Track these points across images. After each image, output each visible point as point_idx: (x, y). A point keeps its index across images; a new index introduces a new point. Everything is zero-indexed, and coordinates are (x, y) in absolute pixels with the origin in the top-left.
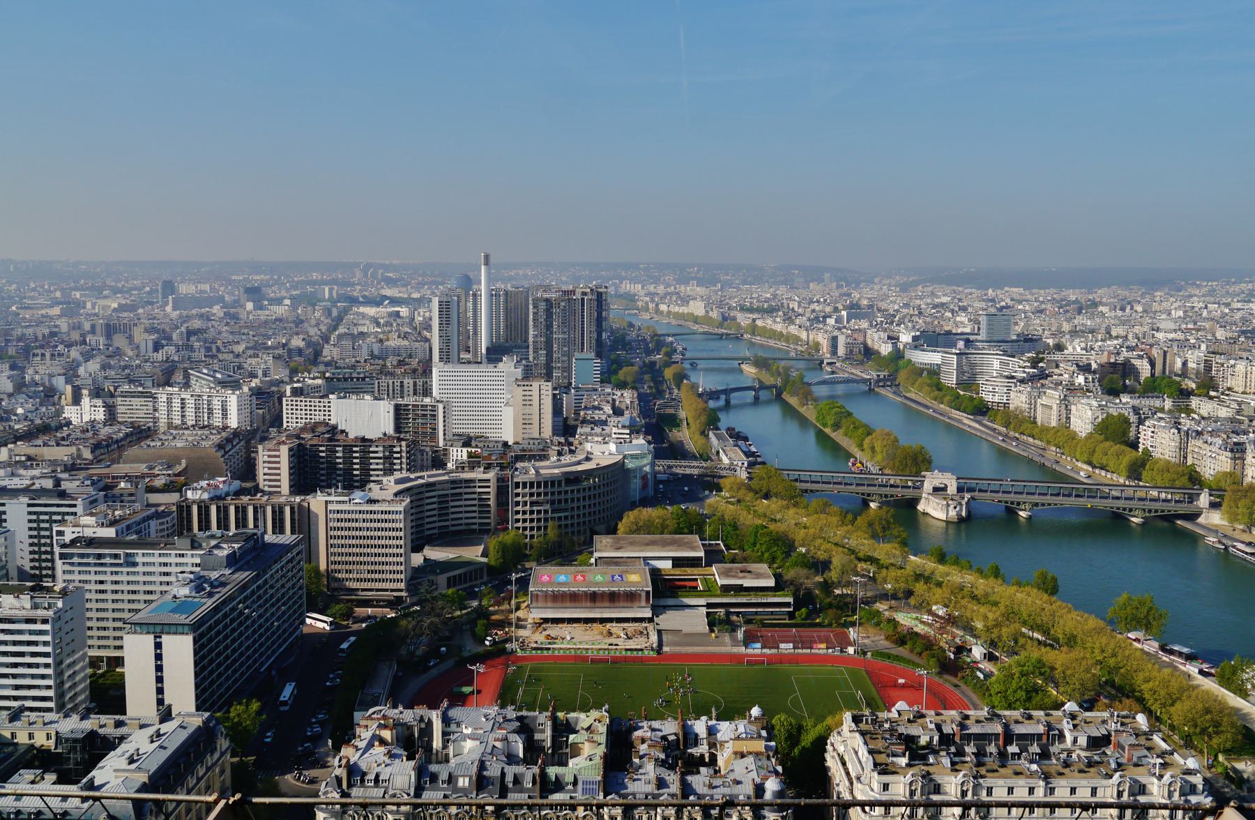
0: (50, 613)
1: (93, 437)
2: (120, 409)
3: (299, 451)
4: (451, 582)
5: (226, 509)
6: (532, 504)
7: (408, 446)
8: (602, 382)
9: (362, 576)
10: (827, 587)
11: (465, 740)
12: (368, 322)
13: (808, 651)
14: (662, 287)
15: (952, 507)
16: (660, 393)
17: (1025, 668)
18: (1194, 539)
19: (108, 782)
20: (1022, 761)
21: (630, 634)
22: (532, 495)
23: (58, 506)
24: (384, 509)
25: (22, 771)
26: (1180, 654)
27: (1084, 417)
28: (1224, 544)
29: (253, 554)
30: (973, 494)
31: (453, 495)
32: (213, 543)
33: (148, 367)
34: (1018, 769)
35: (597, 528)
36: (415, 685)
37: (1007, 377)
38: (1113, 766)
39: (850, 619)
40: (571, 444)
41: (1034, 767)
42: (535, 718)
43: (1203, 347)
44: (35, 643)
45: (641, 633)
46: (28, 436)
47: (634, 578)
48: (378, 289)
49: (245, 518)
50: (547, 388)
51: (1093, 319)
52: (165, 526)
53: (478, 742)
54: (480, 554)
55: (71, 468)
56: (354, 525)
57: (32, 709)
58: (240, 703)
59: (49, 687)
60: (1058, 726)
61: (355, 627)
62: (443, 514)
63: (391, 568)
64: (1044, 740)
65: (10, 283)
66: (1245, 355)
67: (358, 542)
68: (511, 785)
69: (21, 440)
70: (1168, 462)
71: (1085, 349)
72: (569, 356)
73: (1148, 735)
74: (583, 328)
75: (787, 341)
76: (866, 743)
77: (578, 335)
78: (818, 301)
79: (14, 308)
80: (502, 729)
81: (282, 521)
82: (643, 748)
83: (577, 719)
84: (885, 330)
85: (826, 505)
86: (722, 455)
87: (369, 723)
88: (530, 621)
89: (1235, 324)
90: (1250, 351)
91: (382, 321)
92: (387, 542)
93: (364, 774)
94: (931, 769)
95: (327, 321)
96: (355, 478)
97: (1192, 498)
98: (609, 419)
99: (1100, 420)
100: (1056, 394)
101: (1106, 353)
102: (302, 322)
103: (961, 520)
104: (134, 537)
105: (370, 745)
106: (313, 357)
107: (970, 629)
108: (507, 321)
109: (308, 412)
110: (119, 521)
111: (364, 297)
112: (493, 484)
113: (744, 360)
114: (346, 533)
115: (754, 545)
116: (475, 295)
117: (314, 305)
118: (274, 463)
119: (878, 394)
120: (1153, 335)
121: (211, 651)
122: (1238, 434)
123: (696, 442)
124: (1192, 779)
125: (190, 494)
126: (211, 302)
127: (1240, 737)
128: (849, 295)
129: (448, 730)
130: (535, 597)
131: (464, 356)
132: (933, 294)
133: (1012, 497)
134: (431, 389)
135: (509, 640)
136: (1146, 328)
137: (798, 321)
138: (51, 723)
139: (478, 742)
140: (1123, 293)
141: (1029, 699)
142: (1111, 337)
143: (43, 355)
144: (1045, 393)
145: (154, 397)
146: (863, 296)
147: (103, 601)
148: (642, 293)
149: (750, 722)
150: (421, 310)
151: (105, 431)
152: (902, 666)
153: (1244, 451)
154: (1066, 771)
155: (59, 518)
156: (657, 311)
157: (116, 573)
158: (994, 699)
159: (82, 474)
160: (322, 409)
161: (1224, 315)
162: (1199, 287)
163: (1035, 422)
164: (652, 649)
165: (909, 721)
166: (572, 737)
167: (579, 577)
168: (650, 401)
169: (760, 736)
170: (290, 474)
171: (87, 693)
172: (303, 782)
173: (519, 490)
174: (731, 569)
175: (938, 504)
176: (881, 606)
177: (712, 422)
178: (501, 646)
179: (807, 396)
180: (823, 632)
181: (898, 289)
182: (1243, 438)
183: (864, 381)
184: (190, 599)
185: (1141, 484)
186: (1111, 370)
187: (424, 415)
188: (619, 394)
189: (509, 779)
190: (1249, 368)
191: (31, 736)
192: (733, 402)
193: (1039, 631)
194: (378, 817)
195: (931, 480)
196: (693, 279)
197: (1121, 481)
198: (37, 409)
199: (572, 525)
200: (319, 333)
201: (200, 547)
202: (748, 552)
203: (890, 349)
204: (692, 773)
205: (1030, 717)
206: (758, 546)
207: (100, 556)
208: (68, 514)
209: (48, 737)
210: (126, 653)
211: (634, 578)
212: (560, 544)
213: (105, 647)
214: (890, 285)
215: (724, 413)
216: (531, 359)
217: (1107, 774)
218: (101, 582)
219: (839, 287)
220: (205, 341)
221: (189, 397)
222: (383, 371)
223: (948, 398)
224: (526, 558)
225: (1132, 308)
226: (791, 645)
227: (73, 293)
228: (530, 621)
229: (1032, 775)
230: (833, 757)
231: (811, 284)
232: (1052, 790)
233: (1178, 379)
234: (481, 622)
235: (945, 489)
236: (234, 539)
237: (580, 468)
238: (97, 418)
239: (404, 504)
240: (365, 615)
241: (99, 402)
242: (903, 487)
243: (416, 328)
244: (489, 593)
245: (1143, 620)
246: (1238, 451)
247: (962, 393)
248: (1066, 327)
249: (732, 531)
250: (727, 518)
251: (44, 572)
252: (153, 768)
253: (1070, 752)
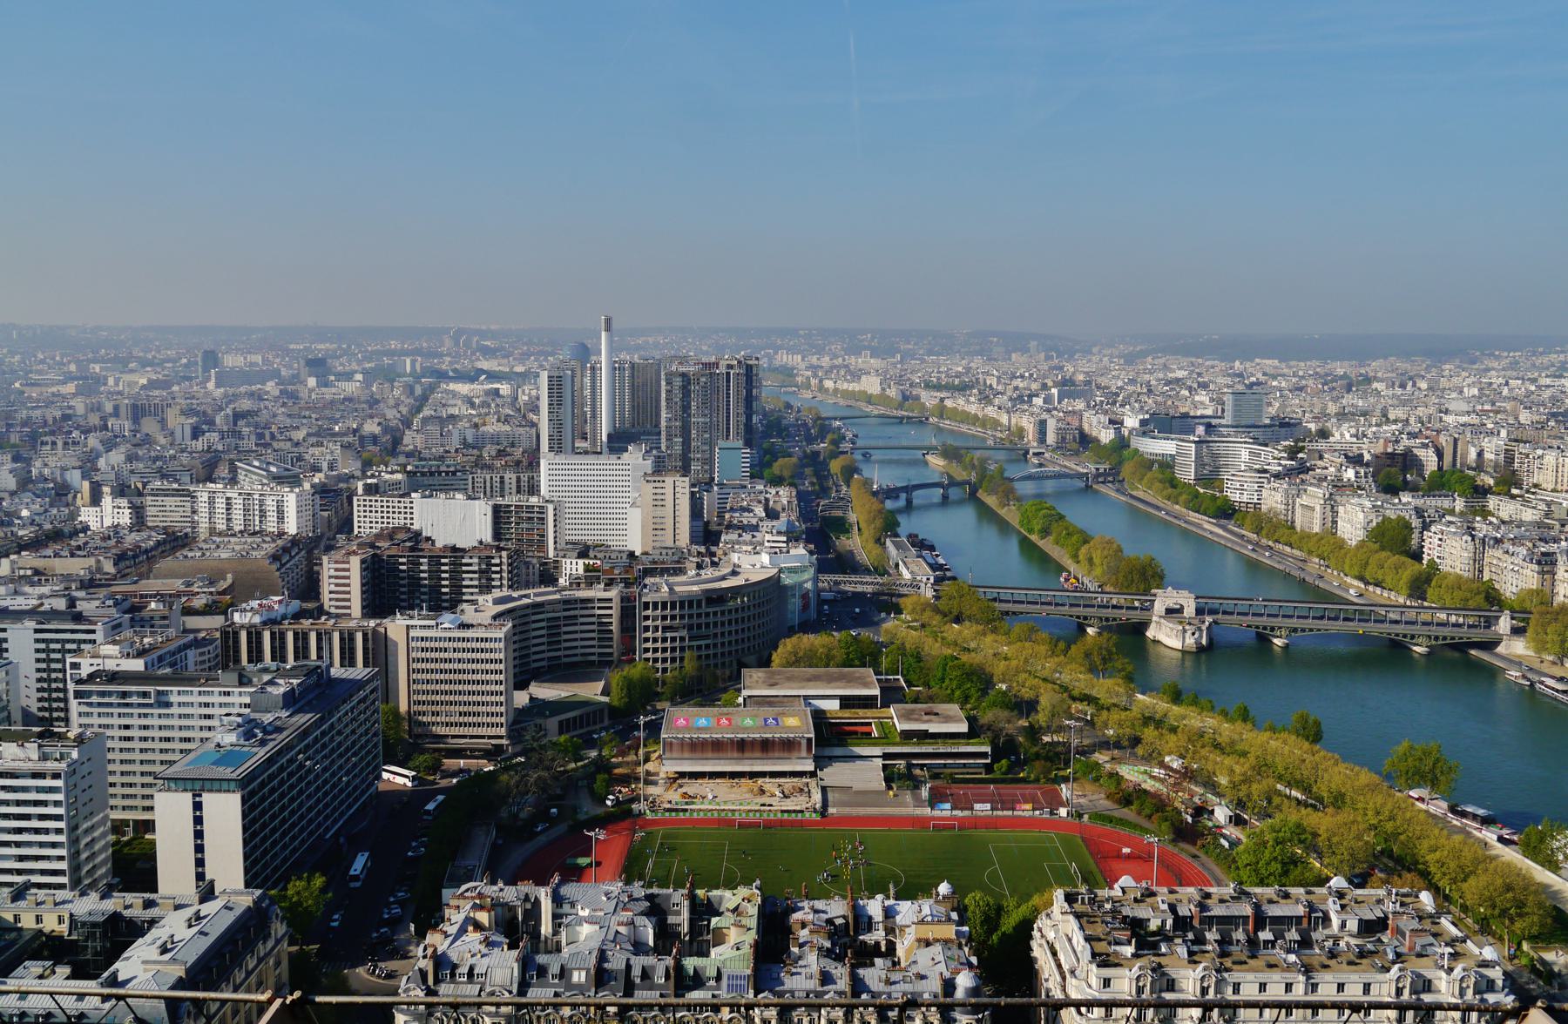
0: (63, 765)
1: (116, 546)
2: (151, 511)
3: (373, 563)
4: (564, 727)
5: (282, 636)
6: (665, 629)
7: (509, 557)
8: (752, 477)
9: (452, 719)
10: (1033, 732)
11: (581, 925)
12: (459, 402)
13: (1010, 813)
14: (827, 359)
15: (1189, 633)
16: (824, 491)
17: (1281, 835)
18: (1491, 673)
19: (135, 977)
20: (1277, 950)
21: (787, 792)
22: (664, 618)
23: (73, 631)
24: (480, 635)
25: (27, 963)
26: (1475, 817)
27: (1354, 521)
28: (1529, 680)
29: (317, 692)
30: (1215, 617)
31: (566, 618)
32: (266, 678)
33: (185, 458)
34: (1272, 960)
35: (746, 660)
36: (518, 855)
37: (1259, 471)
38: (1391, 956)
39: (1062, 773)
40: (713, 554)
41: (1292, 958)
42: (669, 897)
43: (1503, 433)
44: (44, 803)
45: (801, 790)
46: (35, 545)
47: (792, 722)
48: (472, 361)
49: (306, 647)
50: (684, 485)
51: (1365, 398)
52: (206, 657)
53: (597, 927)
54: (599, 692)
56: (442, 655)
57: (40, 886)
58: (300, 878)
59: (61, 858)
60: (1322, 907)
61: (444, 783)
62: (554, 642)
63: (489, 709)
64: (1305, 924)
65: (12, 353)
66: (1555, 443)
67: (447, 676)
68: (638, 981)
69: (26, 550)
70: (1459, 577)
71: (1356, 436)
72: (711, 444)
73: (1434, 918)
74: (728, 409)
75: (984, 426)
76: (1082, 928)
77: (722, 419)
78: (1022, 376)
79: (17, 385)
80: (627, 910)
81: (352, 650)
82: (804, 934)
83: (721, 898)
84: (1106, 412)
85: (1032, 630)
86: (902, 568)
87: (461, 902)
88: (662, 775)
89: (1543, 404)
90: (1562, 438)
91: (477, 401)
92: (484, 677)
93: (455, 967)
94: (1163, 960)
95: (408, 401)
96: (444, 597)
97: (1490, 622)
98: (761, 524)
99: (1374, 524)
100: (1319, 492)
101: (1382, 441)
102: (377, 402)
103: (1201, 649)
104: (168, 670)
105: (462, 931)
106: (392, 445)
107: (1212, 786)
108: (633, 401)
109: (385, 515)
110: (149, 650)
111: (455, 370)
112: (616, 604)
113: (930, 449)
114: (433, 666)
115: (943, 680)
116: (593, 369)
117: (392, 381)
118: (342, 578)
119: (1097, 492)
120: (1441, 418)
121: (263, 813)
122: (1547, 542)
123: (870, 552)
124: (1489, 973)
125: (237, 617)
126: (263, 377)
127: (1549, 921)
128: (1061, 368)
129: (560, 911)
130: (669, 746)
131: (580, 444)
132: (1165, 367)
133: (1264, 621)
134: (539, 486)
135: (636, 799)
136: (1432, 410)
137: (996, 401)
138: (64, 902)
139: (597, 927)
140: (1403, 366)
141: (1286, 873)
142: (1388, 421)
143: (54, 443)
144: (1305, 491)
145: (192, 496)
146: (1078, 370)
147: (128, 750)
148: (802, 366)
149: (937, 902)
150: (526, 388)
151: (131, 539)
152: (1126, 831)
153: (1554, 563)
154: (1332, 963)
155: (74, 646)
156: (821, 388)
157: (146, 716)
158: (1241, 872)
159: (103, 592)
160: (403, 510)
161: (1529, 394)
162: (1498, 358)
163: (1293, 527)
164: (815, 811)
165: (1136, 900)
166: (714, 921)
167: (724, 721)
168: (812, 501)
169: (949, 920)
170: (363, 592)
171: (109, 865)
172: (379, 976)
173: (649, 612)
174: (913, 711)
175: (1172, 629)
176: (1101, 757)
177: (889, 527)
178: (625, 807)
179: (1008, 495)
180: (1028, 789)
181: (1122, 361)
182: (1553, 547)
183: (1080, 476)
184: (237, 748)
185: (1426, 604)
186: (1389, 462)
187: (530, 518)
188: (774, 492)
189: (636, 972)
190: (1561, 460)
191: (39, 919)
192: (915, 502)
193: (1298, 787)
194: (473, 1020)
195: (1164, 599)
196: (866, 348)
197: (1401, 600)
198: (46, 511)
199: (715, 655)
200: (398, 416)
201: (249, 683)
202: (935, 689)
203: (1112, 436)
204: (865, 965)
205: (1287, 896)
206: (947, 681)
207: (124, 695)
208: (85, 641)
209: (60, 920)
211: (792, 722)
212: (699, 680)
213: (131, 808)
214: (1111, 356)
215: (905, 516)
217: (1383, 967)
218: (127, 727)
219: (1048, 358)
220: (257, 426)
221: (236, 495)
222: (479, 464)
223: (1184, 497)
224: (658, 696)
225: (1414, 385)
226: (988, 806)
227: (92, 365)
228: (662, 775)
229: (1289, 967)
230: (1041, 945)
231: (1014, 355)
232: (1314, 987)
233: (1471, 473)
234: (601, 777)
235: (1180, 610)
236: (293, 673)
237: (724, 584)
238: (121, 522)
239: (505, 629)
240: (456, 768)
241: (124, 502)
242: (1128, 608)
243: (519, 410)
244: (611, 741)
245: (1428, 775)
247: (1202, 491)
248: (1332, 408)
249: (914, 663)
250: (908, 646)
251: (55, 715)
252: (191, 960)
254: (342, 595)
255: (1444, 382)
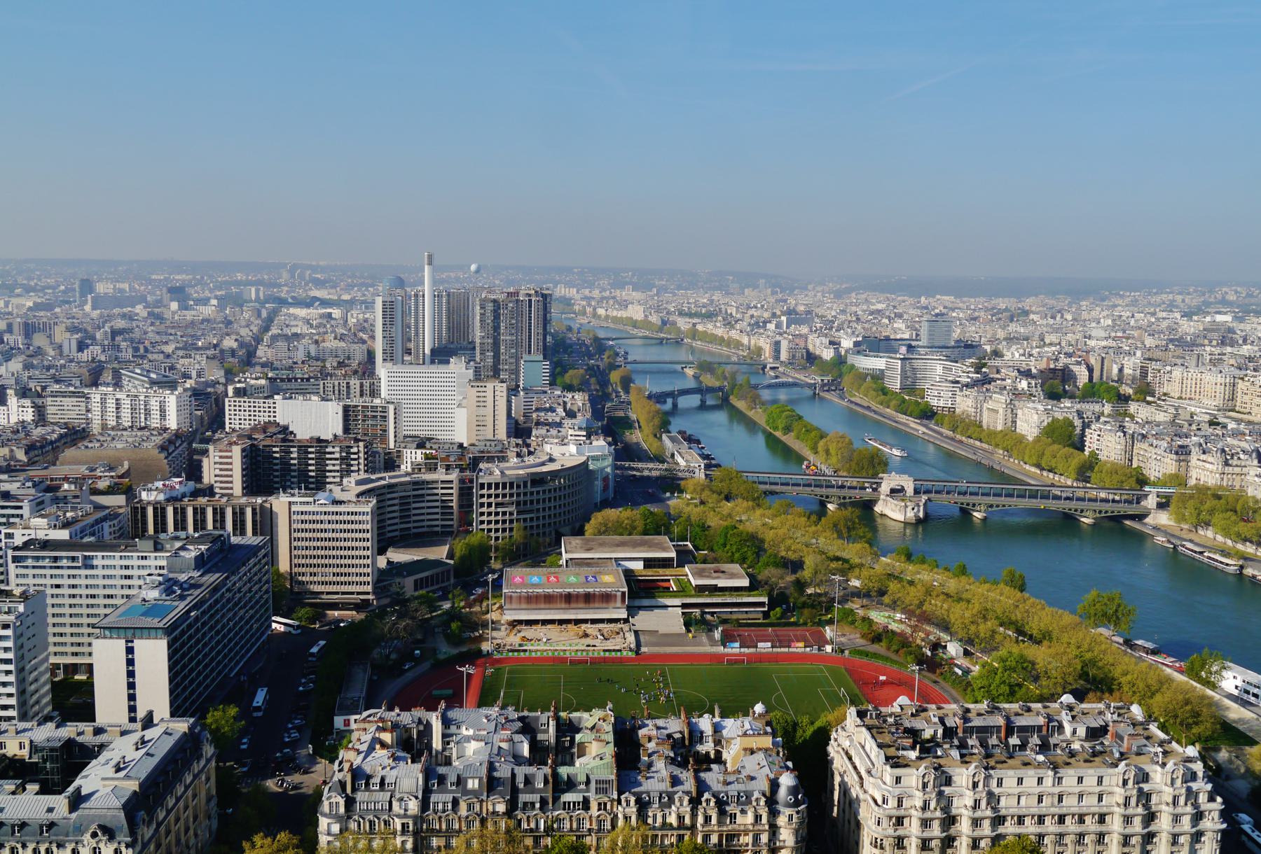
2: (50, 410)
3: (251, 451)
4: (418, 585)
7: (366, 447)
9: (327, 579)
10: (800, 585)
12: (300, 323)
13: (786, 650)
15: (910, 508)
18: (1140, 537)
19: (97, 791)
21: (606, 635)
22: (497, 496)
24: (350, 510)
28: (1172, 544)
29: (221, 556)
31: (415, 496)
32: (178, 544)
35: (562, 530)
38: (1117, 755)
39: (824, 618)
40: (528, 446)
41: (1041, 758)
42: (537, 718)
43: (1139, 353)
47: (608, 579)
49: (204, 521)
50: (502, 389)
51: (1024, 325)
53: (483, 744)
56: (319, 526)
59: (10, 695)
62: (405, 517)
63: (358, 570)
64: (1044, 732)
66: (1179, 361)
68: (521, 786)
73: (1144, 725)
74: (530, 329)
75: (728, 345)
76: (873, 737)
80: (506, 730)
84: (826, 336)
91: (314, 323)
92: (354, 544)
94: (942, 761)
96: (275, 461)
99: (1045, 423)
101: (1045, 359)
103: (919, 521)
104: (92, 539)
105: (371, 749)
107: (946, 627)
111: (293, 298)
114: (311, 535)
115: (725, 545)
117: (241, 306)
118: (225, 465)
119: (822, 399)
121: (184, 655)
128: (785, 301)
131: (407, 358)
133: (968, 499)
136: (1079, 336)
137: (738, 326)
138: (24, 730)
139: (483, 744)
144: (991, 397)
146: (800, 302)
149: (754, 718)
151: (38, 432)
152: (880, 663)
154: (1072, 760)
156: (595, 315)
157: (74, 576)
158: (976, 693)
160: (247, 409)
162: (1122, 297)
163: (981, 427)
164: (631, 650)
165: (912, 715)
167: (552, 578)
169: (766, 733)
170: (243, 476)
173: (485, 492)
174: (703, 570)
176: (855, 605)
179: (755, 401)
180: (799, 631)
181: (832, 296)
184: (160, 602)
185: (1088, 485)
187: (375, 417)
188: (570, 396)
190: (1185, 374)
192: (680, 406)
195: (889, 482)
197: (1069, 483)
199: (538, 526)
200: (251, 334)
201: (162, 550)
205: (1029, 710)
206: (728, 547)
207: (56, 559)
209: (21, 746)
210: (94, 660)
211: (608, 579)
213: (62, 654)
214: (823, 292)
219: (773, 293)
220: (132, 341)
226: (769, 644)
229: (1039, 765)
230: (838, 752)
231: (746, 290)
232: (1060, 779)
233: (1116, 384)
235: (902, 490)
236: (202, 540)
237: (544, 469)
238: (25, 419)
239: (371, 505)
241: (27, 402)
245: (1111, 617)
247: (907, 398)
248: (1001, 334)
250: (693, 518)
252: (143, 776)
254: (226, 478)
255: (1085, 315)
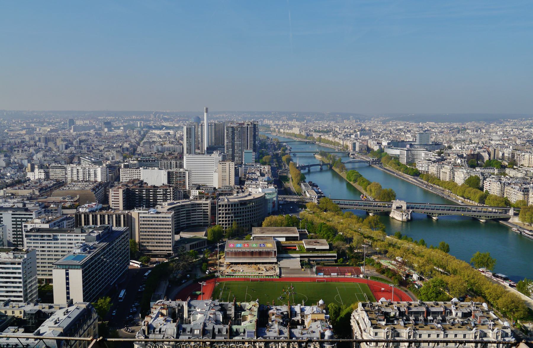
0: (21, 260)
1: (40, 186)
2: (51, 174)
3: (127, 191)
4: (192, 247)
5: (96, 216)
6: (226, 214)
7: (173, 189)
8: (256, 162)
9: (154, 244)
10: (351, 249)
11: (197, 314)
12: (156, 137)
13: (343, 276)
14: (281, 122)
15: (404, 215)
16: (280, 167)
18: (507, 229)
19: (46, 332)
20: (434, 323)
21: (267, 269)
22: (226, 210)
23: (25, 215)
24: (163, 216)
25: (9, 327)
26: (501, 278)
27: (460, 177)
28: (520, 231)
29: (108, 235)
30: (413, 210)
31: (192, 210)
32: (91, 230)
33: (63, 156)
34: (432, 326)
35: (253, 224)
36: (176, 291)
37: (428, 160)
38: (473, 325)
39: (361, 263)
40: (242, 188)
41: (439, 326)
42: (227, 305)
43: (511, 147)
44: (15, 273)
45: (272, 269)
46: (12, 185)
47: (269, 245)
48: (161, 123)
49: (104, 220)
50: (232, 165)
51: (464, 135)
52: (70, 223)
53: (203, 315)
54: (204, 235)
55: (30, 199)
56: (150, 223)
57: (13, 301)
58: (102, 298)
59: (21, 292)
60: (449, 308)
61: (151, 266)
62: (188, 218)
63: (166, 241)
64: (444, 314)
65: (4, 120)
66: (529, 151)
67: (152, 230)
68: (217, 333)
69: (9, 187)
70: (496, 196)
71: (461, 148)
72: (242, 151)
73: (487, 312)
74: (248, 139)
75: (334, 145)
76: (368, 315)
77: (245, 142)
78: (347, 128)
79: (6, 131)
80: (213, 309)
81: (120, 221)
82: (273, 318)
83: (245, 305)
84: (376, 140)
85: (351, 214)
86: (307, 193)
87: (157, 307)
88: (225, 263)
89: (525, 137)
91: (162, 136)
92: (165, 230)
93: (155, 329)
94: (395, 326)
95: (139, 136)
96: (151, 203)
97: (506, 211)
98: (259, 178)
99: (467, 178)
100: (448, 167)
101: (470, 150)
102: (128, 137)
103: (408, 221)
104: (57, 228)
105: (157, 316)
106: (133, 151)
107: (412, 267)
108: (215, 136)
109: (131, 175)
110: (51, 221)
111: (155, 126)
112: (209, 205)
114: (147, 226)
115: (320, 231)
116: (202, 125)
117: (133, 129)
118: (116, 197)
119: (373, 167)
120: (490, 142)
121: (89, 276)
122: (526, 184)
123: (296, 188)
124: (506, 331)
125: (80, 210)
126: (89, 128)
127: (527, 313)
128: (361, 125)
129: (190, 310)
130: (227, 253)
131: (197, 151)
132: (396, 125)
133: (430, 211)
134: (183, 165)
135: (216, 272)
136: (487, 139)
137: (339, 136)
138: (22, 307)
139: (203, 315)
140: (477, 124)
141: (437, 297)
142: (472, 143)
143: (18, 151)
144: (444, 167)
145: (65, 169)
146: (366, 126)
147: (44, 255)
148: (273, 124)
149: (318, 306)
150: (179, 132)
151: (45, 183)
152: (383, 283)
153: (528, 191)
154: (453, 327)
155: (25, 220)
156: (279, 132)
157: (49, 243)
158: (422, 296)
159: (35, 201)
160: (137, 173)
161: (520, 134)
162: (509, 122)
163: (439, 179)
164: (277, 276)
165: (386, 306)
166: (243, 313)
167: (246, 245)
168: (276, 170)
169: (323, 313)
170: (123, 201)
171: (37, 294)
172: (129, 332)
173: (221, 208)
174: (310, 242)
175: (398, 214)
176: (374, 257)
177: (302, 179)
178: (213, 274)
179: (343, 168)
180: (350, 268)
181: (381, 123)
182: (528, 186)
183: (367, 162)
184: (81, 254)
185: (485, 205)
186: (472, 157)
187: (180, 176)
188: (263, 167)
189: (216, 330)
190: (531, 156)
191: (13, 312)
192: (311, 171)
194: (161, 347)
195: (396, 204)
196: (294, 118)
197: (476, 204)
198: (16, 174)
199: (243, 223)
200: (135, 141)
201: (85, 232)
202: (318, 234)
203: (378, 148)
204: (294, 328)
205: (437, 304)
206: (322, 232)
207: (42, 236)
208: (29, 218)
209: (21, 313)
211: (269, 245)
212: (238, 231)
213: (45, 275)
214: (378, 121)
215: (308, 175)
216: (226, 152)
217: (470, 328)
218: (43, 247)
219: (356, 122)
220: (87, 145)
221: (80, 168)
222: (163, 158)
223: (403, 169)
224: (224, 237)
225: (481, 131)
226: (336, 274)
227: (31, 124)
228: (225, 263)
229: (438, 329)
230: (354, 321)
231: (345, 121)
232: (447, 335)
233: (500, 161)
234: (204, 264)
235: (401, 207)
236: (100, 229)
237: (246, 199)
238: (41, 177)
239: (172, 214)
240: (155, 261)
241: (42, 171)
242: (383, 207)
243: (177, 139)
244: (208, 252)
245: (486, 263)
246: (526, 191)
247: (408, 167)
248: (453, 139)
249: (311, 225)
250: (309, 220)
251: (19, 243)
252: (65, 326)
253: (454, 319)
255: (491, 130)
